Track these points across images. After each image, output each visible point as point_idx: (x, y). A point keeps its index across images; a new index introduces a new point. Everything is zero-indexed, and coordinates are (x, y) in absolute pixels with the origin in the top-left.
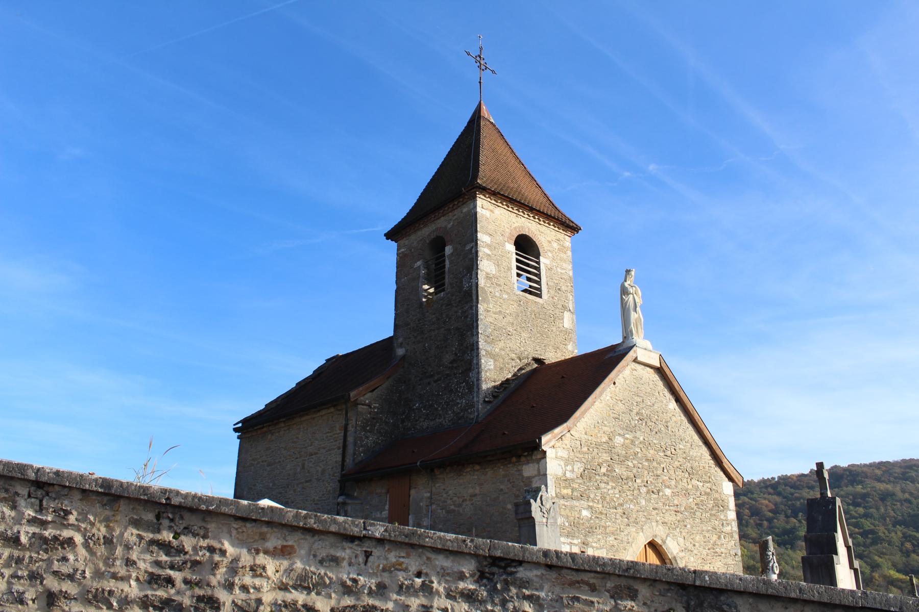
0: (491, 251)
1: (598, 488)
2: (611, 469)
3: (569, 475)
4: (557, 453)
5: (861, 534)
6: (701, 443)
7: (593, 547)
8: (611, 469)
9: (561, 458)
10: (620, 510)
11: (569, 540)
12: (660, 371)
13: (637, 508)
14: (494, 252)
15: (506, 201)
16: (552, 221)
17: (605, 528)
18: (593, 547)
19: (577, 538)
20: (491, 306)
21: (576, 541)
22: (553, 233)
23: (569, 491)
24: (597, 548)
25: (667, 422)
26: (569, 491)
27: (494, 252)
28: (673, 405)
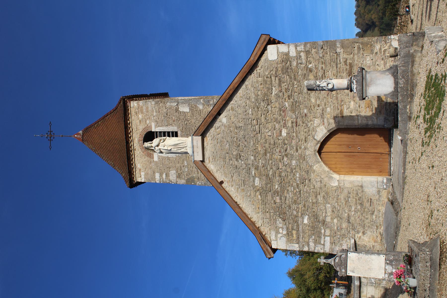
1: (290, 207)
2: (276, 193)
3: (285, 232)
4: (273, 240)
5: (319, 287)
6: (244, 86)
7: (325, 216)
8: (276, 193)
9: (276, 236)
10: (301, 186)
11: (323, 237)
12: (203, 135)
13: (298, 169)
14: (163, 170)
15: (130, 162)
16: (129, 146)
17: (313, 203)
18: (325, 216)
19: (321, 229)
20: (195, 175)
21: (323, 231)
22: (133, 117)
23: (294, 232)
24: (326, 213)
26: (294, 232)
27: (163, 170)
28: (223, 118)
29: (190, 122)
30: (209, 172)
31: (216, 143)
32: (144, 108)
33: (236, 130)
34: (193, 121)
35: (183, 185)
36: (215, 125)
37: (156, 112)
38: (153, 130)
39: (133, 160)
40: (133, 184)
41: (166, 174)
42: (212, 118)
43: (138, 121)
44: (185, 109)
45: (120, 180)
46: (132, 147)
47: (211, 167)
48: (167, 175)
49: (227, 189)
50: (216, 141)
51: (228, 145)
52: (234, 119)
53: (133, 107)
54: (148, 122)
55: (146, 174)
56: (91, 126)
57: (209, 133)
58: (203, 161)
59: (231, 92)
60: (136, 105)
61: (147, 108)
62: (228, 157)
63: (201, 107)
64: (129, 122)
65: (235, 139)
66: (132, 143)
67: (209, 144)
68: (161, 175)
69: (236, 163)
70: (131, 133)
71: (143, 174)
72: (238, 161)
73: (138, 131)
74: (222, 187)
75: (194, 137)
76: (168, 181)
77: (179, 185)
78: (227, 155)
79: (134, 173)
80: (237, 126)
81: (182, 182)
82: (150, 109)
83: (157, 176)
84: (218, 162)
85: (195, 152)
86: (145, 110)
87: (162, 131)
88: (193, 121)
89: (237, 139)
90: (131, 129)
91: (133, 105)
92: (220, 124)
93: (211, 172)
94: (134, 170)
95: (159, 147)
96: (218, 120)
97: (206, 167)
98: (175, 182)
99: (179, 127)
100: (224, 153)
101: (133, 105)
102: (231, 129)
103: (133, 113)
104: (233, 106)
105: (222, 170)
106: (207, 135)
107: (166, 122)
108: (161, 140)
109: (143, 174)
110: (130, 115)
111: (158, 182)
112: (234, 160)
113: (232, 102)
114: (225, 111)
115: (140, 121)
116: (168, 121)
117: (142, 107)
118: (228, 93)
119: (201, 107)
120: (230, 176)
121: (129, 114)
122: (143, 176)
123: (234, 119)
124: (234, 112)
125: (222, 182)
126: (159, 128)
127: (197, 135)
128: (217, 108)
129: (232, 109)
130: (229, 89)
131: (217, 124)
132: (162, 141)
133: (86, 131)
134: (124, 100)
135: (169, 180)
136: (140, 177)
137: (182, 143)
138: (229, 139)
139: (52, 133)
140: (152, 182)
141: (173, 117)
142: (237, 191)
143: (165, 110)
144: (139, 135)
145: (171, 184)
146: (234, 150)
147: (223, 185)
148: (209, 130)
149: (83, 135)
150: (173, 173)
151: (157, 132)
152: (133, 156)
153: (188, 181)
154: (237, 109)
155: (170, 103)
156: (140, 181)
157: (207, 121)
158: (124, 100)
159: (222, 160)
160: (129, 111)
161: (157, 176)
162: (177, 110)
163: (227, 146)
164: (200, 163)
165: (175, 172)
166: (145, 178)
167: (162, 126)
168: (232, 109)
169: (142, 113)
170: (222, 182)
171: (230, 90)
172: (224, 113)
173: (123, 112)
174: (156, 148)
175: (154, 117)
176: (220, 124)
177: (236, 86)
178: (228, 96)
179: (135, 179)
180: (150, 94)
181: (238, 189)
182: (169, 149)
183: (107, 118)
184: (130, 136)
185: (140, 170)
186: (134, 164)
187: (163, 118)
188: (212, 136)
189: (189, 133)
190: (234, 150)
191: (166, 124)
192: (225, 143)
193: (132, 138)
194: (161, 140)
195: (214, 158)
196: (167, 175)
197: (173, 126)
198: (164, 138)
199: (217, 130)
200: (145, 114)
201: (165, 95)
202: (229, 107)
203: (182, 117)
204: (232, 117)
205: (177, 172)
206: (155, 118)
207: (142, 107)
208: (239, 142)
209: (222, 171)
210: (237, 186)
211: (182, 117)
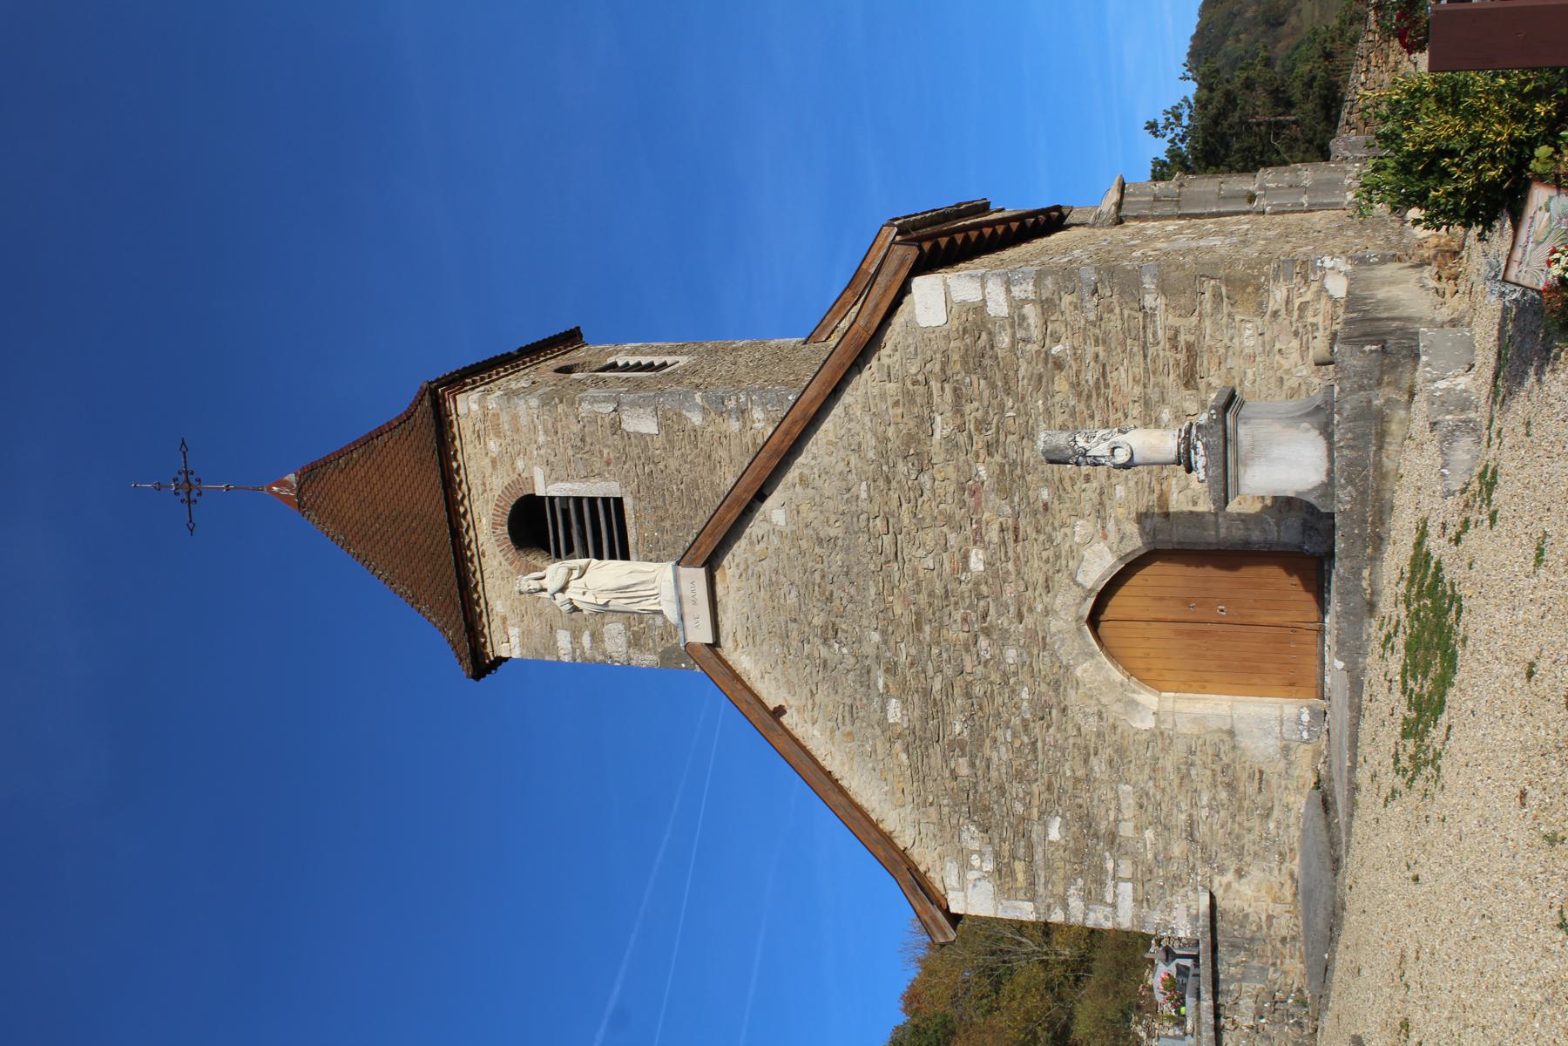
0: (581, 632)
12: (711, 564)
22: (469, 449)
25: (820, 541)
28: (774, 511)
29: (661, 466)
30: (737, 677)
31: (755, 589)
32: (505, 418)
33: (817, 550)
34: (673, 464)
35: (650, 668)
36: (748, 531)
37: (546, 432)
38: (540, 492)
39: (480, 588)
40: (482, 665)
41: (592, 635)
42: (736, 512)
43: (487, 461)
44: (642, 423)
45: (435, 644)
46: (473, 546)
47: (743, 661)
48: (596, 638)
49: (798, 732)
50: (753, 581)
51: (794, 593)
52: (812, 515)
53: (467, 415)
54: (520, 464)
55: (526, 634)
56: (325, 462)
57: (729, 557)
58: (715, 645)
59: (797, 431)
60: (475, 407)
61: (515, 417)
62: (795, 633)
63: (696, 419)
64: (455, 465)
65: (817, 576)
66: (471, 533)
67: (732, 592)
68: (576, 637)
69: (824, 651)
70: (466, 502)
71: (514, 632)
72: (830, 647)
73: (489, 495)
74: (781, 725)
75: (682, 570)
76: (600, 658)
77: (638, 669)
78: (792, 626)
79: (486, 631)
80: (822, 535)
81: (648, 659)
82: (524, 421)
83: (563, 639)
84: (765, 647)
85: (686, 618)
86: (506, 426)
87: (570, 494)
88: (673, 464)
89: (823, 577)
90: (464, 486)
91: (467, 406)
92: (766, 526)
93: (745, 678)
94: (484, 619)
95: (569, 594)
96: (758, 516)
97: (724, 662)
98: (623, 658)
99: (625, 485)
100: (782, 619)
101: (467, 406)
102: (804, 544)
103: (468, 434)
104: (806, 471)
105: (777, 673)
106: (725, 562)
107: (580, 466)
108: (571, 570)
109: (514, 632)
110: (457, 443)
111: (566, 659)
112: (818, 641)
113: (801, 460)
114: (780, 487)
115: (494, 462)
116: (587, 463)
117: (496, 416)
118: (787, 433)
119: (696, 419)
120: (806, 690)
121: (454, 439)
122: (514, 640)
123: (812, 515)
124: (810, 492)
125: (780, 711)
126: (560, 485)
127: (691, 564)
128: (753, 481)
129: (803, 481)
130: (789, 419)
131: (755, 528)
132: (576, 574)
133: (309, 474)
134: (434, 393)
135: (604, 653)
136: (507, 641)
137: (642, 583)
138: (796, 576)
139: (192, 479)
140: (547, 658)
141: (605, 451)
142: (832, 738)
143: (576, 428)
144: (491, 506)
145: (612, 666)
146: (815, 611)
147: (785, 719)
148: (730, 547)
149: (300, 489)
150: (614, 633)
151: (552, 499)
152: (478, 575)
153: (666, 656)
154: (818, 483)
155: (591, 403)
156: (504, 655)
157: (721, 520)
158: (434, 393)
159: (775, 641)
160: (455, 429)
161: (563, 639)
162: (616, 427)
163: (792, 599)
164: (707, 652)
165: (621, 627)
166: (522, 646)
167: (569, 478)
168: (803, 481)
169: (498, 434)
170: (780, 711)
171: (794, 422)
172: (775, 494)
173: (433, 434)
174: (558, 595)
175: (539, 448)
176: (766, 526)
177: (814, 410)
178: (788, 442)
179: (489, 649)
180: (521, 350)
181: (832, 731)
182: (601, 602)
183: (379, 442)
184: (462, 510)
185: (504, 619)
186: (482, 601)
187: (570, 452)
188: (742, 566)
189: (660, 503)
190: (815, 611)
191: (583, 473)
192: (785, 589)
193: (469, 517)
194: (571, 570)
195: (751, 634)
196: (596, 638)
197: (606, 480)
198: (584, 561)
199: (757, 548)
200: (508, 440)
201: (571, 338)
202: (793, 474)
203: (635, 452)
204: (804, 508)
205: (628, 627)
206: (542, 452)
207: (496, 416)
208: (830, 587)
209: (779, 676)
210: (830, 724)
211: (635, 452)
